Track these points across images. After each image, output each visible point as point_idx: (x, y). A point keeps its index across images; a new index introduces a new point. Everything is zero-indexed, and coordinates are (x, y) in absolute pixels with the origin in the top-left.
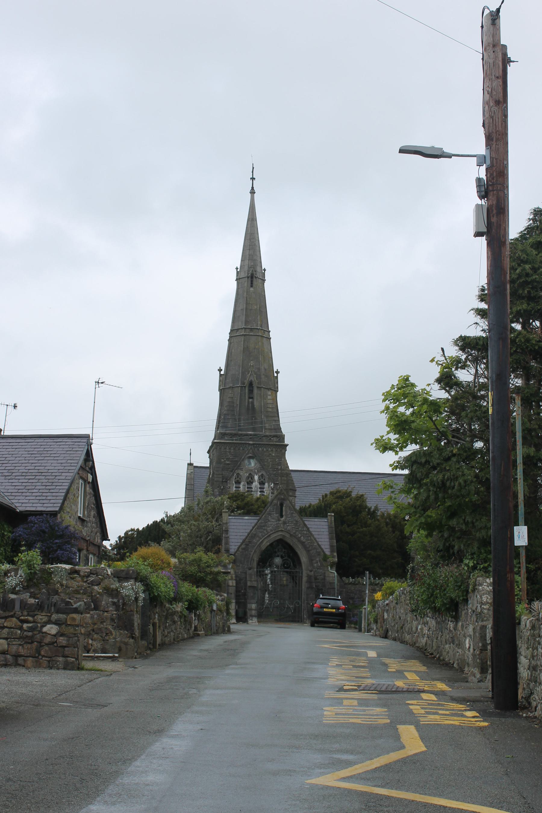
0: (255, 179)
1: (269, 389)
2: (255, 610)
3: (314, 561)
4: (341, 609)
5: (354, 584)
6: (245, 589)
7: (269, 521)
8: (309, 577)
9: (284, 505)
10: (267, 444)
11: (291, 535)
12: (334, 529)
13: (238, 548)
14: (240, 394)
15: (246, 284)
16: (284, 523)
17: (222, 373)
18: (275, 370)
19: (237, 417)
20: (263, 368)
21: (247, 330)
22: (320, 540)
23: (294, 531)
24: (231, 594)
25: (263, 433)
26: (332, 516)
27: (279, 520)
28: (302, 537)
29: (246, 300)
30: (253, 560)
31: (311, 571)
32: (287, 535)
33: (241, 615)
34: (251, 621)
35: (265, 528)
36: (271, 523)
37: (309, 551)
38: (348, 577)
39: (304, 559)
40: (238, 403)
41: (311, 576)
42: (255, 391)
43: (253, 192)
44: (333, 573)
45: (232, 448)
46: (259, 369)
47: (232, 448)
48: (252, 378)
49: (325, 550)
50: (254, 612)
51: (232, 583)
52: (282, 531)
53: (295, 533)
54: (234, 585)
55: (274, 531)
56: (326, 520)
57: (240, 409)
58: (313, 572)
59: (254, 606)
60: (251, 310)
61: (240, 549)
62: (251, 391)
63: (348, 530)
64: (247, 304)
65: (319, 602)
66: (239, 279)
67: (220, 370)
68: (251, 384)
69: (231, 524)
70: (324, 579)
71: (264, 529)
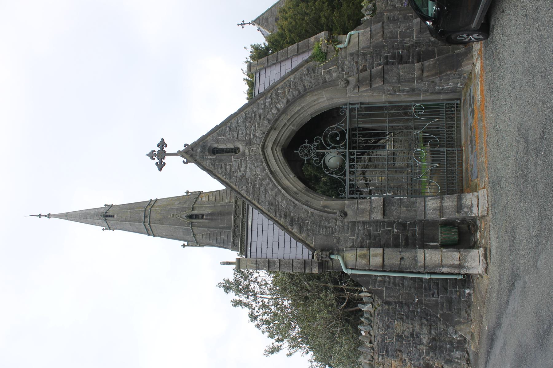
1: (197, 199)
2: (442, 199)
6: (391, 224)
7: (243, 176)
9: (215, 145)
11: (272, 128)
13: (299, 240)
15: (112, 222)
16: (249, 143)
17: (186, 243)
18: (185, 194)
19: (219, 230)
24: (402, 258)
25: (233, 204)
27: (244, 154)
28: (278, 106)
30: (325, 207)
33: (453, 236)
34: (475, 210)
36: (248, 170)
37: (305, 90)
39: (322, 101)
40: (206, 229)
41: (358, 80)
42: (195, 212)
43: (49, 216)
46: (178, 209)
48: (184, 216)
50: (450, 202)
51: (375, 256)
52: (263, 147)
53: (269, 121)
54: (380, 251)
55: (265, 165)
57: (212, 228)
58: (350, 79)
64: (125, 221)
67: (184, 246)
68: (191, 217)
69: (259, 255)
70: (364, 55)
71: (261, 185)
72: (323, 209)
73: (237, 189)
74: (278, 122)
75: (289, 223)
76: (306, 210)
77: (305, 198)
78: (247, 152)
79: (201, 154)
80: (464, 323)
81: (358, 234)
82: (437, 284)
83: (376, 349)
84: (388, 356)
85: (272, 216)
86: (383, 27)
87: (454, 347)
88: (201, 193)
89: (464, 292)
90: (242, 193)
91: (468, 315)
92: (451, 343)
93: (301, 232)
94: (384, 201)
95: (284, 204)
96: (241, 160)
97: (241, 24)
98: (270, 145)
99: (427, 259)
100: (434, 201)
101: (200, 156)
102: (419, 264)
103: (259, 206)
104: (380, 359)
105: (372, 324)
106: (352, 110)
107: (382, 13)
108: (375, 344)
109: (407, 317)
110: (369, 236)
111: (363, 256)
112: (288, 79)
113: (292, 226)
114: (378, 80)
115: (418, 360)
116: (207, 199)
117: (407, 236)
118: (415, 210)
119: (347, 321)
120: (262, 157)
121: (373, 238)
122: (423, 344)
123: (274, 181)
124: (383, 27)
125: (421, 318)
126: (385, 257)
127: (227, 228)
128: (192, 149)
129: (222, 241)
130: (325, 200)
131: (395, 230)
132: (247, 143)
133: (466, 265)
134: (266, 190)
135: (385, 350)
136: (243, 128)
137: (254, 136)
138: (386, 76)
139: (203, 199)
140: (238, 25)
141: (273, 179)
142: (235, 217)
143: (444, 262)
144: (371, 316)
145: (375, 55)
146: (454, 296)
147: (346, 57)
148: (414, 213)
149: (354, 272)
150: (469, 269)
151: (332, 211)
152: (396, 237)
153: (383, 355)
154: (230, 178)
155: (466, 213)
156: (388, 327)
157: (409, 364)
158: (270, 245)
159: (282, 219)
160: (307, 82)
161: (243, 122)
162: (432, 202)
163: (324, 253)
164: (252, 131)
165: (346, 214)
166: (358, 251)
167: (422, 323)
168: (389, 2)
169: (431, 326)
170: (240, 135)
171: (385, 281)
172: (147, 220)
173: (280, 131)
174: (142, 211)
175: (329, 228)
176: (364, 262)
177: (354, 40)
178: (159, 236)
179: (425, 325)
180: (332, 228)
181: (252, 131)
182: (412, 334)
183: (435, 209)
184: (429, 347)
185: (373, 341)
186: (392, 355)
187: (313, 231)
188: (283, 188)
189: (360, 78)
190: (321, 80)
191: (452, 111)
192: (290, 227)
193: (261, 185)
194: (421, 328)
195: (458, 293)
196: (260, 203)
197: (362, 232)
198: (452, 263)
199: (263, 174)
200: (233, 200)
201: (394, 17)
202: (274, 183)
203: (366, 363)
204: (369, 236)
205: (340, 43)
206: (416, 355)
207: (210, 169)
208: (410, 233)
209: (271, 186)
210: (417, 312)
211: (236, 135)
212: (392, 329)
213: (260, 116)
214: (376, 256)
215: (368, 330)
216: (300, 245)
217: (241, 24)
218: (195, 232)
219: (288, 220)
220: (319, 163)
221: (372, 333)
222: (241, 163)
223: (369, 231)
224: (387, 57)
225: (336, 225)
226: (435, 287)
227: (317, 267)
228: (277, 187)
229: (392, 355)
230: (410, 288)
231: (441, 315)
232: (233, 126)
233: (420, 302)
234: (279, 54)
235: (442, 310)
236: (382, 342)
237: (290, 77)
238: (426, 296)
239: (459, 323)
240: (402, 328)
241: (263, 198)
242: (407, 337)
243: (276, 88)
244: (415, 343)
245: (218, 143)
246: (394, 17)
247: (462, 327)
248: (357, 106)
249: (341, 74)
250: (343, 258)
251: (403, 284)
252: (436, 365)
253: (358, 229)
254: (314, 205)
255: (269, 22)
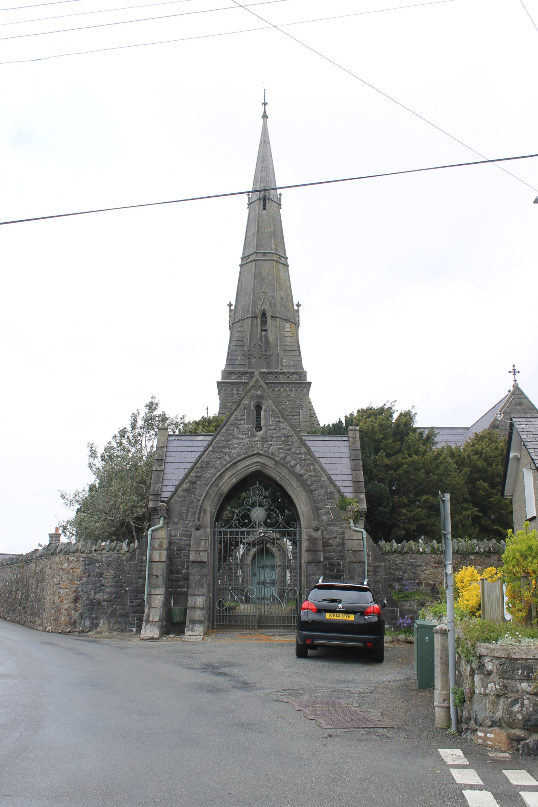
0: (267, 104)
2: (202, 609)
3: (323, 511)
4: (367, 613)
5: (400, 553)
7: (234, 437)
8: (312, 540)
9: (263, 408)
10: (284, 383)
11: (276, 463)
12: (359, 452)
13: (177, 488)
14: (251, 325)
15: (257, 208)
16: (264, 440)
17: (233, 308)
18: (295, 303)
20: (278, 296)
21: (259, 254)
22: (333, 472)
23: (282, 455)
24: (157, 577)
25: (279, 370)
26: (356, 430)
27: (254, 436)
28: (298, 466)
29: (258, 223)
30: (205, 511)
31: (317, 530)
32: (270, 463)
34: (190, 633)
35: (228, 451)
37: (311, 491)
38: (388, 540)
40: (248, 337)
41: (316, 539)
43: (265, 116)
44: (358, 535)
45: (241, 390)
46: (274, 297)
47: (241, 390)
48: (264, 307)
49: (343, 490)
50: (198, 614)
51: (160, 555)
52: (258, 454)
53: (284, 458)
54: (164, 559)
55: (243, 456)
56: (345, 439)
58: (320, 532)
59: (200, 601)
60: (263, 233)
61: (180, 492)
62: (264, 322)
63: (387, 461)
64: (258, 227)
65: (316, 597)
66: (251, 204)
68: (264, 315)
70: (343, 545)
71: (225, 453)
72: (202, 510)
73: (222, 431)
74: (282, 467)
75: (192, 480)
76: (202, 494)
77: (213, 493)
78: (256, 439)
79: (255, 395)
80: (109, 626)
81: (181, 540)
82: (140, 606)
83: (90, 555)
84: (85, 565)
85: (197, 465)
86: (359, 562)
87: (93, 620)
88: (296, 324)
89: (134, 627)
90: (219, 436)
91: (116, 630)
92: (96, 618)
93: (183, 491)
94: (204, 562)
95: (207, 475)
96: (248, 434)
97: (514, 370)
98: (261, 460)
99: (156, 597)
100: (201, 602)
101: (254, 394)
102: (152, 590)
103: (206, 453)
104: (82, 559)
105: (111, 552)
106: (295, 534)
107: (383, 561)
108: (95, 555)
109: (117, 582)
110: (180, 549)
111: (161, 545)
112: (323, 474)
113: (189, 482)
114: (311, 557)
115: (82, 591)
116: (287, 334)
117: (179, 581)
118: (196, 588)
119: (122, 525)
120: (251, 453)
121: (178, 552)
122: (95, 595)
123: (227, 466)
124: (359, 562)
125: (117, 593)
126: (159, 563)
127: (250, 363)
128: (260, 386)
129: (234, 358)
130: (211, 512)
131: (184, 571)
132: (264, 438)
133: (149, 626)
134: (220, 458)
135: (90, 563)
136: (278, 434)
137: (271, 445)
138: (313, 565)
139: (287, 330)
140: (514, 366)
141: (230, 464)
142: (264, 373)
143: (152, 610)
144: (118, 551)
145: (342, 554)
146: (130, 619)
147: (341, 528)
148: (194, 586)
149: (149, 537)
150: (145, 627)
151: (201, 517)
152: (178, 572)
153: (85, 561)
154: (232, 425)
155: (188, 627)
156: (109, 566)
157: (79, 583)
158: (177, 460)
159: (194, 474)
160: (319, 493)
161: (284, 434)
162: (201, 601)
163: (165, 512)
164: (274, 443)
165: (198, 529)
166: (166, 540)
167: (112, 594)
168: (409, 567)
169: (110, 601)
170: (271, 431)
171: (142, 563)
172: (260, 257)
173: (274, 469)
174: (271, 249)
175: (187, 515)
176: (156, 545)
177: (356, 536)
178: (241, 272)
179: (111, 597)
180: (187, 518)
181: (274, 443)
182: (103, 585)
183: (195, 603)
184: (93, 600)
185: (97, 552)
186: (86, 569)
187: (184, 501)
188: (221, 474)
189: (317, 541)
190: (320, 505)
191: (291, 622)
192: (188, 481)
193: (225, 453)
194: (108, 593)
195: (132, 622)
196: (209, 453)
197: (183, 543)
198: (151, 615)
199: (234, 455)
200: (285, 370)
201: (379, 572)
202: (226, 465)
203: (79, 546)
204: (180, 549)
205: (355, 523)
206: (86, 589)
207: (241, 405)
208: (182, 583)
209: (224, 462)
210: (121, 590)
211: (272, 428)
212: (107, 569)
213: (288, 450)
214: (161, 556)
215: (106, 548)
216: (173, 489)
217: (514, 370)
218: (245, 321)
219: (194, 479)
220: (246, 504)
221: (104, 551)
222: (245, 434)
223: (184, 549)
224: (339, 565)
225: (189, 521)
226: (138, 603)
227: (153, 506)
228: (223, 468)
229: (86, 569)
230: (137, 583)
231: (115, 608)
232: (281, 425)
233: (126, 591)
234: (358, 461)
235: (120, 609)
236: (96, 560)
237: (325, 476)
238: (130, 596)
239: (109, 623)
240: (108, 577)
241: (214, 455)
242: (100, 581)
243: (315, 463)
244: (96, 588)
245: (266, 410)
246: (379, 572)
247: (107, 625)
248: (298, 537)
249: (325, 523)
250: (161, 528)
251: (140, 578)
252: (79, 606)
253: (185, 540)
254: (206, 502)
255: (517, 407)
